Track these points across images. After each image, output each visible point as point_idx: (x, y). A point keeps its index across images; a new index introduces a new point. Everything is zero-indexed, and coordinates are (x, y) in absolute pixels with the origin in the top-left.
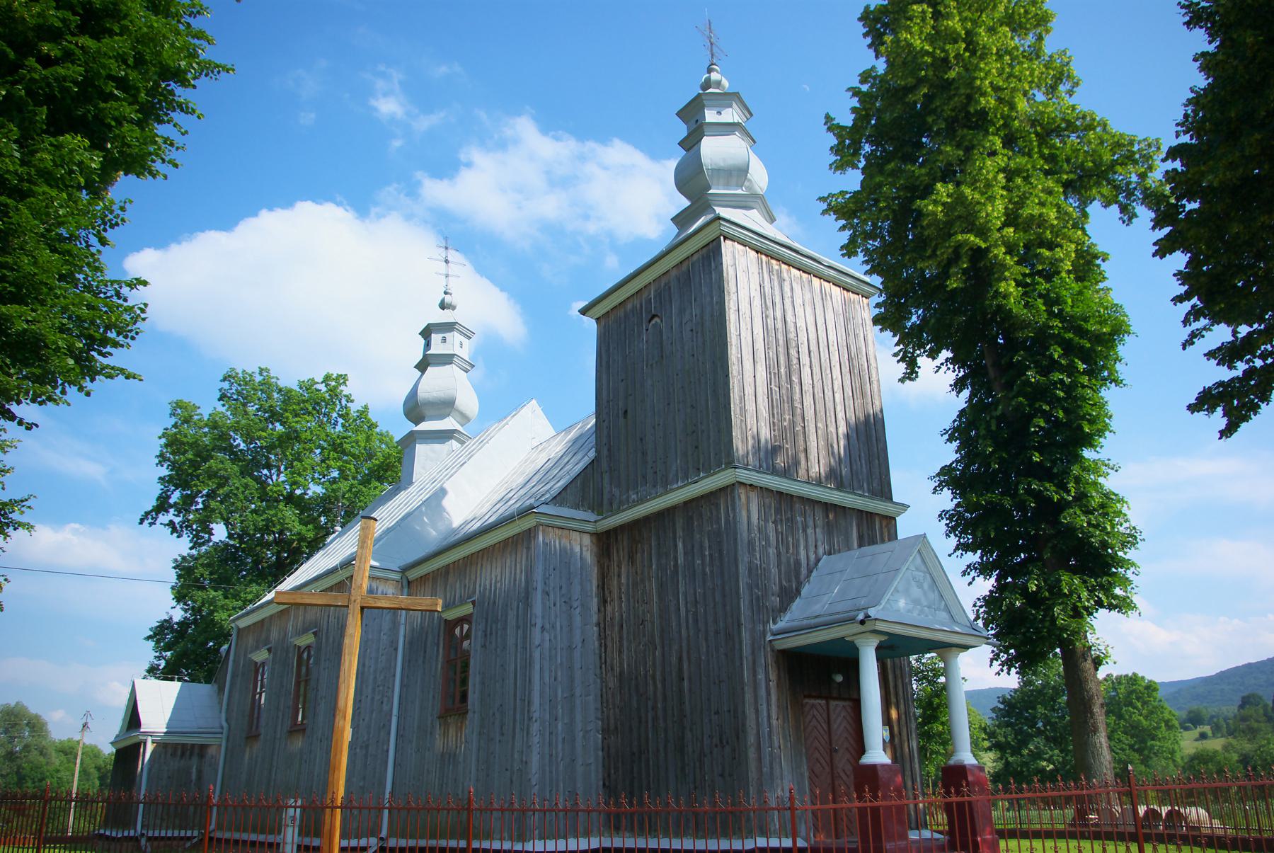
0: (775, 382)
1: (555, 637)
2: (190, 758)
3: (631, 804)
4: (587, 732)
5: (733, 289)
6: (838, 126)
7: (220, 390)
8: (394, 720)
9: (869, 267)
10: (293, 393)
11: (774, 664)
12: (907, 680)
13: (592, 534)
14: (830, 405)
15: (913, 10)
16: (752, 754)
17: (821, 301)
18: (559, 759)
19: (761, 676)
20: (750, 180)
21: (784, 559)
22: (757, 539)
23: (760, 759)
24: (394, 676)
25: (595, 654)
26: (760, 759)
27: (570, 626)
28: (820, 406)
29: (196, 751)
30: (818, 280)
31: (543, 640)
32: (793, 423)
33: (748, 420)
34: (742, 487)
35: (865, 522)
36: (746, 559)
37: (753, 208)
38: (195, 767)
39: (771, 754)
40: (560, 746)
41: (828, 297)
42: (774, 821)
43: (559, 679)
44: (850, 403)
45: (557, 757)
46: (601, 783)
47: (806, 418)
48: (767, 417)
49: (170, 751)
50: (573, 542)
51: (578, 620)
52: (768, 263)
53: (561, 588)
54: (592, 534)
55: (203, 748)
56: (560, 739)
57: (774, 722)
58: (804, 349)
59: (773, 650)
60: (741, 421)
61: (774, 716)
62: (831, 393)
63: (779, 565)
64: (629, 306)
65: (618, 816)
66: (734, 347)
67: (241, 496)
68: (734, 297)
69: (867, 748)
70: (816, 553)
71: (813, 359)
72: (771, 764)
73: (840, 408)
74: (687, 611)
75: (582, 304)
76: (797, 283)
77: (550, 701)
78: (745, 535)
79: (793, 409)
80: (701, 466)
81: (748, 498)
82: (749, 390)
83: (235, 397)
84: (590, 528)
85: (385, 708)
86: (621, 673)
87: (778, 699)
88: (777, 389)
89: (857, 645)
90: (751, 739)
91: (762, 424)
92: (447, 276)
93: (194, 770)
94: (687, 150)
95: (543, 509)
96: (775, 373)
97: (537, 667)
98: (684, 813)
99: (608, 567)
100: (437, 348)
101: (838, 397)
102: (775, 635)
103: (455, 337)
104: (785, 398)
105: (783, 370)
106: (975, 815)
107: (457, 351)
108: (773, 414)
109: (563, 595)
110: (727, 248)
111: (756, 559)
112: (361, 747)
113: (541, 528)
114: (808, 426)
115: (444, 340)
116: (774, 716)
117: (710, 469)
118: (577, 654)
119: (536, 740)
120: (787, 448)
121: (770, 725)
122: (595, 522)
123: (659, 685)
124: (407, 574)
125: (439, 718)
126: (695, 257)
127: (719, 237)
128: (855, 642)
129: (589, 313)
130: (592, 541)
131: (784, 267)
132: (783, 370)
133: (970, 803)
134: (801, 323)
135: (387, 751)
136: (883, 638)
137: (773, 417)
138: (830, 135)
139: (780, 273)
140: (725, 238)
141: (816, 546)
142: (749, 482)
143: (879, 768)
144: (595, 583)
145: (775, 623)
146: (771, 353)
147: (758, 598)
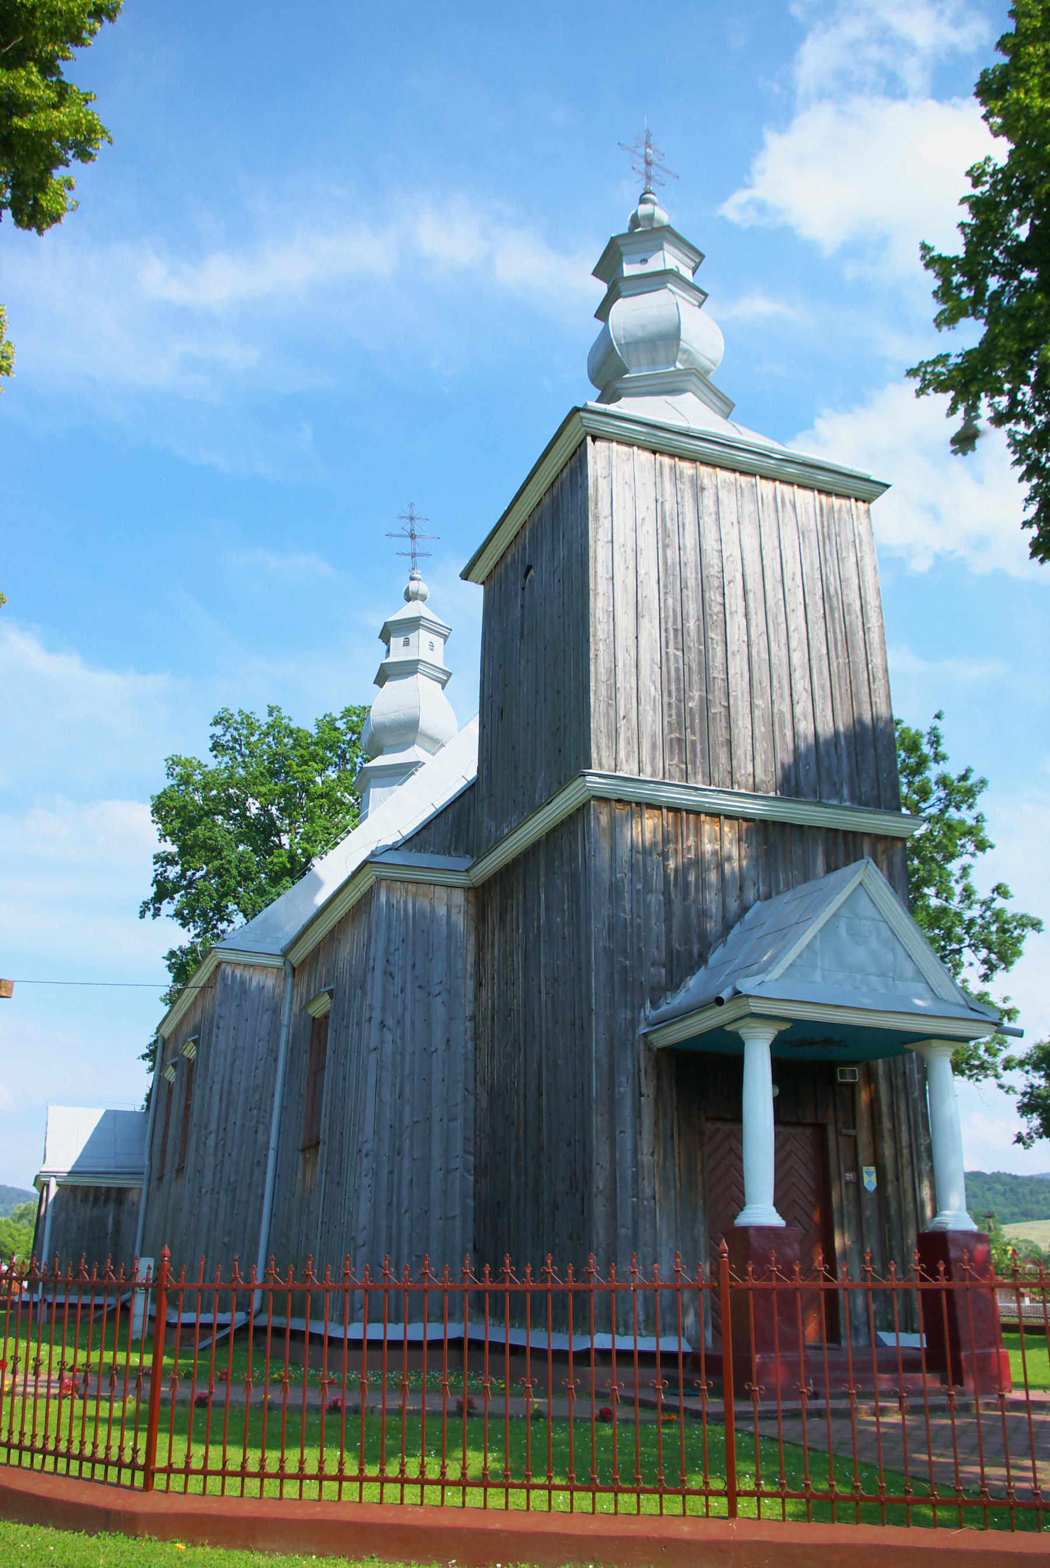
0: (676, 643)
1: (402, 1037)
2: (105, 1205)
3: (520, 1274)
4: (448, 1171)
6: (941, 259)
7: (212, 737)
8: (272, 1154)
9: (1024, 467)
10: (301, 734)
11: (650, 1070)
12: (916, 1094)
13: (467, 889)
15: (1029, 54)
16: (599, 1208)
17: (773, 515)
18: (403, 1211)
19: (625, 1089)
20: (685, 351)
21: (677, 909)
22: (626, 882)
23: (613, 1215)
24: (273, 1096)
25: (466, 1059)
26: (613, 1215)
27: (428, 1021)
28: (761, 674)
29: (113, 1195)
31: (383, 1042)
32: (706, 703)
33: (622, 704)
34: (603, 805)
35: (842, 847)
36: (605, 912)
38: (111, 1216)
39: (635, 1208)
40: (405, 1192)
41: (789, 507)
42: (634, 1309)
43: (407, 1094)
44: (820, 666)
46: (470, 1245)
47: (732, 694)
48: (658, 697)
49: (79, 1196)
50: (436, 903)
51: (440, 1012)
52: (673, 468)
53: (414, 966)
54: (467, 889)
55: (122, 1192)
57: (646, 1159)
58: (734, 591)
59: (649, 1048)
60: (609, 705)
61: (646, 1146)
62: (784, 652)
63: (668, 919)
64: (509, 558)
65: (480, 1294)
66: (600, 598)
67: (234, 872)
68: (605, 523)
69: (747, 1200)
70: (740, 898)
71: (751, 604)
72: (635, 1223)
75: (461, 568)
78: (606, 876)
79: (707, 682)
81: (688, 818)
82: (625, 659)
83: (231, 744)
84: (461, 879)
85: (261, 1138)
86: (492, 1086)
87: (656, 1123)
88: (680, 653)
90: (600, 1182)
91: (646, 707)
92: (413, 555)
93: (110, 1220)
96: (676, 630)
98: (392, 1292)
100: (399, 653)
103: (422, 637)
104: (694, 666)
105: (692, 625)
106: (959, 1314)
107: (424, 654)
109: (417, 977)
110: (596, 452)
111: (624, 911)
112: (226, 1191)
113: (384, 883)
114: (736, 704)
115: (407, 643)
116: (646, 1146)
117: (562, 783)
118: (437, 1061)
120: (693, 743)
121: (636, 1163)
122: (467, 871)
125: (303, 1150)
126: (564, 474)
128: (740, 1032)
129: (471, 576)
130: (466, 899)
131: (704, 469)
132: (692, 625)
133: (950, 1293)
134: (731, 549)
135: (263, 1196)
136: (788, 1026)
137: (670, 695)
138: (931, 273)
140: (594, 439)
141: (741, 888)
142: (615, 796)
143: (751, 1231)
144: (471, 958)
145: (655, 1005)
146: (670, 602)
147: (624, 971)
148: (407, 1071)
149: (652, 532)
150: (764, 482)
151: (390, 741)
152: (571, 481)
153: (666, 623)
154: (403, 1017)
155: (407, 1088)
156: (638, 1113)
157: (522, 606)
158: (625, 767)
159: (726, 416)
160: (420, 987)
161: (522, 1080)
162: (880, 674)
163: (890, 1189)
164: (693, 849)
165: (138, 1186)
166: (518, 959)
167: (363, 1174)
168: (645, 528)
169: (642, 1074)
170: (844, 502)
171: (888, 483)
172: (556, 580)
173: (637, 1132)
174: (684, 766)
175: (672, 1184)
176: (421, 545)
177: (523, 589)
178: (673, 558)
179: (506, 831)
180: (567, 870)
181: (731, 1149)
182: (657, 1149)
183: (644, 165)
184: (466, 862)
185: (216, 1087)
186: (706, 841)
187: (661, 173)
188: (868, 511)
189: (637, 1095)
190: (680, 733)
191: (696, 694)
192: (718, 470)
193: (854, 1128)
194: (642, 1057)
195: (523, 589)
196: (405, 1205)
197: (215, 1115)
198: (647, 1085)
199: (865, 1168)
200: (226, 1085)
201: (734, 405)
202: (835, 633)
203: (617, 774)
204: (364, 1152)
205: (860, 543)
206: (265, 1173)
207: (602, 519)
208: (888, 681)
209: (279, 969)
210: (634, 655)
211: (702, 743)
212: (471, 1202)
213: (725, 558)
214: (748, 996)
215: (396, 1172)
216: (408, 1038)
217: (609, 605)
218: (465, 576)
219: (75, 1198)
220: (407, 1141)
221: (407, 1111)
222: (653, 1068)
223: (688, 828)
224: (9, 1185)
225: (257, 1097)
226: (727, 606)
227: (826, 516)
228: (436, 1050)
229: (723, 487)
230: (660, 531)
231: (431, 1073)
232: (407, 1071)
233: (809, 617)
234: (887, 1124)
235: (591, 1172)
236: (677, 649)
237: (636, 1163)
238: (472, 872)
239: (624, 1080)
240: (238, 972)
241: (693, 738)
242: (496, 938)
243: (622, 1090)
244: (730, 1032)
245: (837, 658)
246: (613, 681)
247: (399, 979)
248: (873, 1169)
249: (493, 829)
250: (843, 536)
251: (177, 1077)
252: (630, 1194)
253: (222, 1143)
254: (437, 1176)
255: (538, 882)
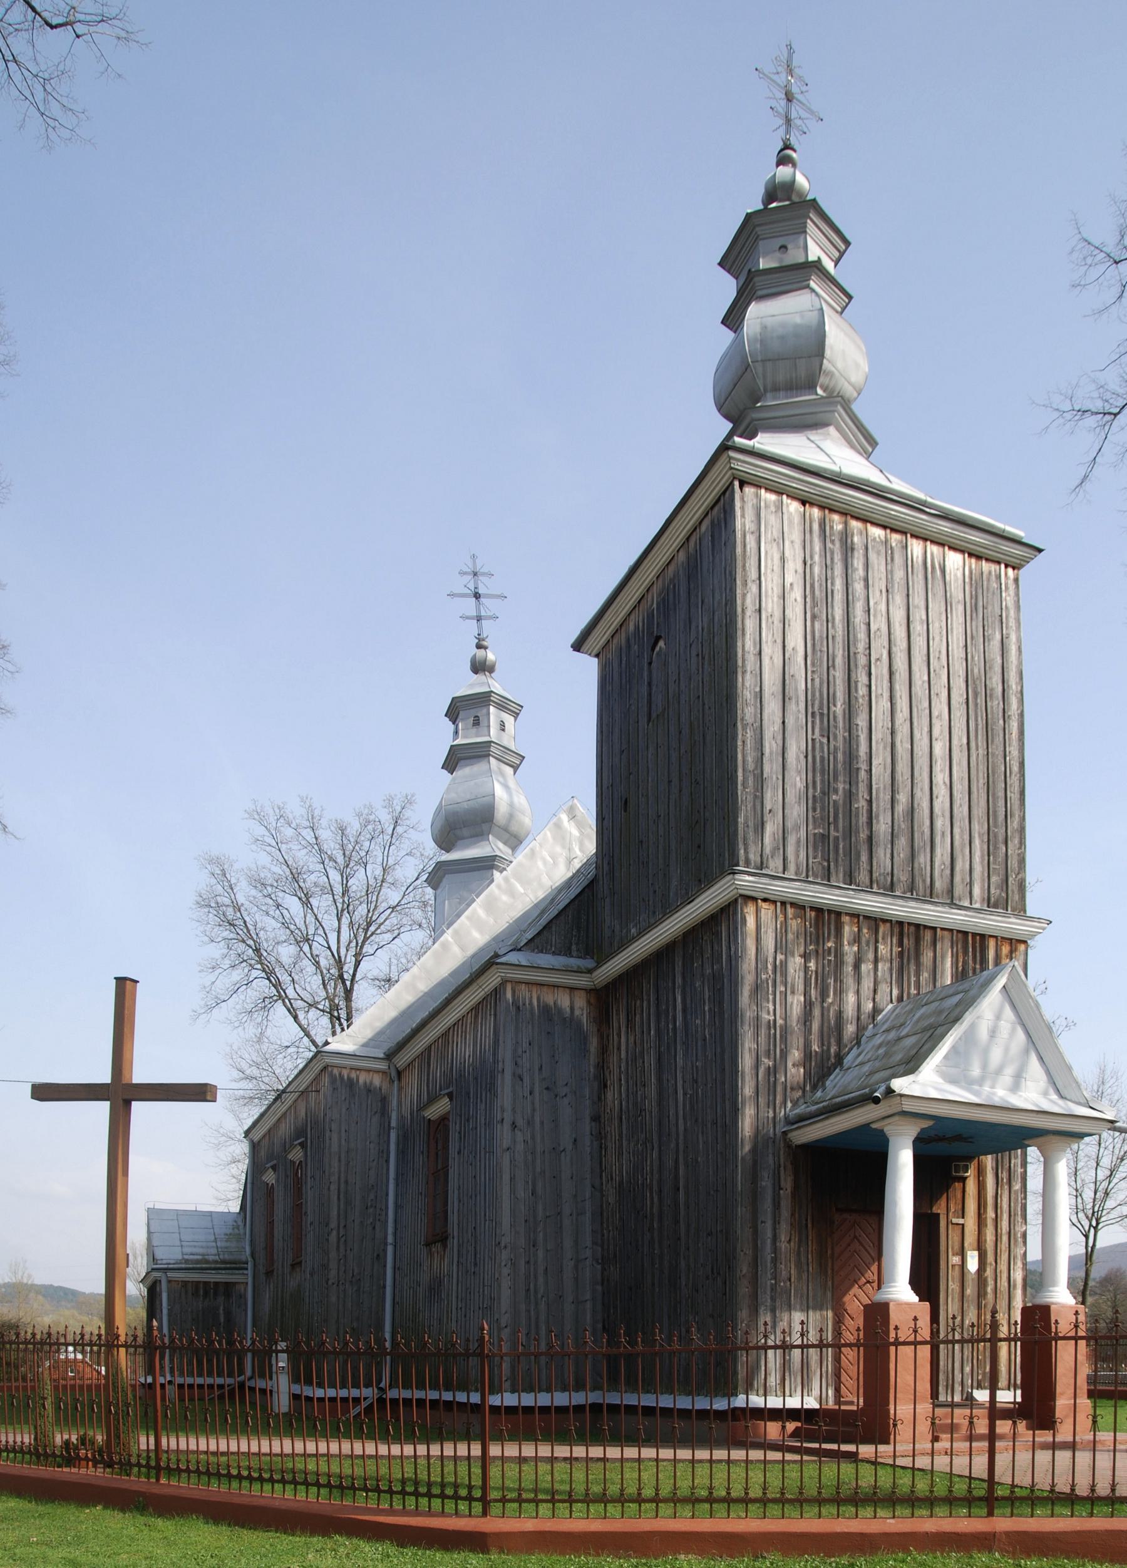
0: (821, 729)
1: (533, 1137)
5: (753, 574)
8: (390, 1249)
11: (789, 1166)
14: (922, 762)
19: (766, 1183)
24: (387, 1195)
28: (903, 767)
30: (921, 542)
31: (514, 1142)
32: (850, 796)
37: (825, 425)
38: (222, 1308)
40: (541, 1280)
44: (959, 756)
45: (536, 1292)
46: (600, 1326)
53: (541, 1069)
54: (589, 991)
56: (541, 1270)
58: (880, 671)
60: (756, 797)
61: (783, 1237)
62: (926, 741)
66: (748, 676)
73: (940, 766)
74: (685, 1094)
76: (878, 553)
77: (526, 1221)
80: (703, 876)
84: (583, 981)
86: (621, 1183)
88: (825, 740)
89: (887, 1133)
92: (479, 619)
93: (221, 1311)
94: (735, 332)
95: (513, 958)
97: (506, 1177)
99: (608, 1036)
101: (940, 749)
102: (793, 1124)
105: (839, 708)
108: (814, 783)
109: (544, 1079)
110: (745, 501)
111: (769, 1013)
114: (878, 798)
115: (477, 722)
117: (704, 880)
119: (505, 1271)
121: (775, 1250)
123: (656, 1200)
124: (395, 1060)
126: (704, 527)
127: (731, 484)
128: (885, 1130)
129: (585, 647)
131: (855, 524)
134: (878, 623)
135: (384, 1287)
136: (926, 1124)
139: (846, 535)
140: (742, 484)
146: (817, 681)
148: (538, 1170)
149: (800, 599)
150: (914, 541)
151: (465, 832)
152: (712, 536)
153: (813, 705)
154: (533, 1116)
155: (540, 1185)
156: (777, 1205)
157: (650, 684)
158: (772, 864)
159: (868, 456)
160: (547, 1089)
161: (656, 1176)
162: (1016, 769)
163: (989, 1272)
164: (833, 950)
165: (246, 1279)
166: (651, 1060)
167: (503, 1264)
168: (793, 595)
169: (782, 1168)
170: (993, 567)
171: (1041, 547)
172: (694, 653)
173: (776, 1222)
174: (826, 864)
175: (805, 1268)
176: (489, 606)
177: (650, 664)
178: (821, 631)
179: (633, 931)
180: (708, 971)
181: (855, 1237)
182: (793, 1237)
183: (783, 103)
184: (589, 963)
185: (333, 1187)
186: (846, 943)
187: (804, 115)
188: (1016, 580)
189: (777, 1188)
190: (824, 828)
191: (841, 786)
192: (869, 525)
193: (963, 1217)
194: (782, 1152)
195: (650, 664)
196: (541, 1291)
197: (334, 1213)
198: (785, 1180)
199: (969, 1253)
200: (342, 1186)
201: (877, 444)
202: (976, 720)
203: (764, 872)
204: (503, 1245)
205: (1007, 617)
206: (385, 1266)
207: (749, 583)
208: (1023, 775)
209: (384, 1073)
210: (780, 743)
211: (844, 840)
212: (599, 1288)
213: (872, 632)
214: (901, 1095)
215: (532, 1263)
216: (538, 1140)
217: (756, 686)
218: (578, 646)
219: (186, 1292)
220: (541, 1234)
221: (540, 1208)
222: (792, 1164)
223: (829, 929)
224: (56, 1285)
225: (372, 1196)
226: (873, 688)
227: (976, 585)
228: (564, 1150)
229: (873, 547)
230: (808, 600)
231: (560, 1171)
232: (538, 1170)
233: (953, 702)
234: (990, 1214)
235: (734, 1258)
236: (823, 736)
237: (775, 1250)
238: (595, 974)
239: (766, 1175)
240: (345, 1073)
241: (836, 834)
242: (623, 1040)
243: (764, 1184)
244: (875, 1129)
245: (977, 749)
246: (759, 771)
247: (527, 1079)
248: (976, 1253)
249: (617, 928)
250: (990, 608)
251: (277, 1180)
252: (769, 1276)
253: (343, 1239)
254: (568, 1266)
255: (674, 983)
